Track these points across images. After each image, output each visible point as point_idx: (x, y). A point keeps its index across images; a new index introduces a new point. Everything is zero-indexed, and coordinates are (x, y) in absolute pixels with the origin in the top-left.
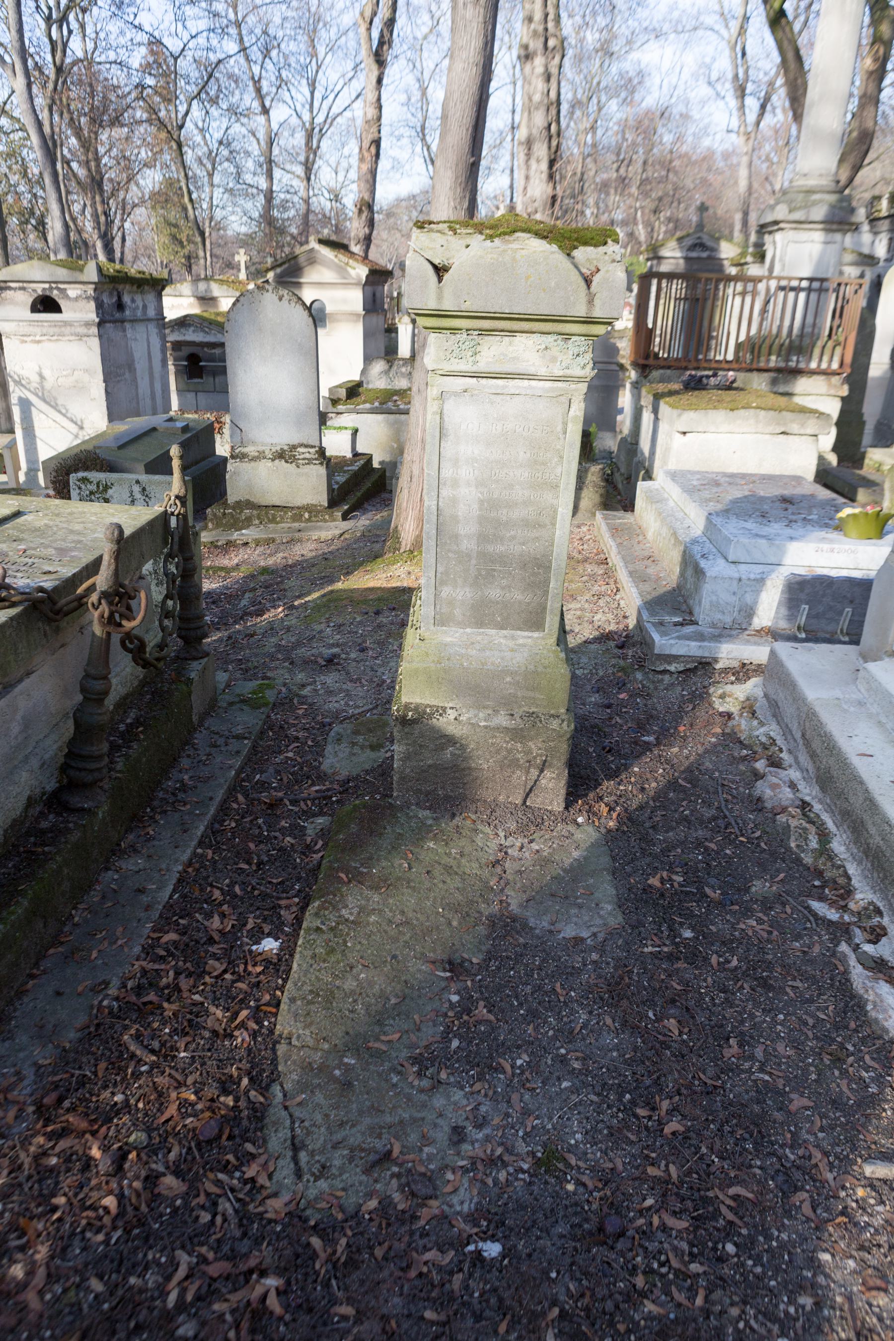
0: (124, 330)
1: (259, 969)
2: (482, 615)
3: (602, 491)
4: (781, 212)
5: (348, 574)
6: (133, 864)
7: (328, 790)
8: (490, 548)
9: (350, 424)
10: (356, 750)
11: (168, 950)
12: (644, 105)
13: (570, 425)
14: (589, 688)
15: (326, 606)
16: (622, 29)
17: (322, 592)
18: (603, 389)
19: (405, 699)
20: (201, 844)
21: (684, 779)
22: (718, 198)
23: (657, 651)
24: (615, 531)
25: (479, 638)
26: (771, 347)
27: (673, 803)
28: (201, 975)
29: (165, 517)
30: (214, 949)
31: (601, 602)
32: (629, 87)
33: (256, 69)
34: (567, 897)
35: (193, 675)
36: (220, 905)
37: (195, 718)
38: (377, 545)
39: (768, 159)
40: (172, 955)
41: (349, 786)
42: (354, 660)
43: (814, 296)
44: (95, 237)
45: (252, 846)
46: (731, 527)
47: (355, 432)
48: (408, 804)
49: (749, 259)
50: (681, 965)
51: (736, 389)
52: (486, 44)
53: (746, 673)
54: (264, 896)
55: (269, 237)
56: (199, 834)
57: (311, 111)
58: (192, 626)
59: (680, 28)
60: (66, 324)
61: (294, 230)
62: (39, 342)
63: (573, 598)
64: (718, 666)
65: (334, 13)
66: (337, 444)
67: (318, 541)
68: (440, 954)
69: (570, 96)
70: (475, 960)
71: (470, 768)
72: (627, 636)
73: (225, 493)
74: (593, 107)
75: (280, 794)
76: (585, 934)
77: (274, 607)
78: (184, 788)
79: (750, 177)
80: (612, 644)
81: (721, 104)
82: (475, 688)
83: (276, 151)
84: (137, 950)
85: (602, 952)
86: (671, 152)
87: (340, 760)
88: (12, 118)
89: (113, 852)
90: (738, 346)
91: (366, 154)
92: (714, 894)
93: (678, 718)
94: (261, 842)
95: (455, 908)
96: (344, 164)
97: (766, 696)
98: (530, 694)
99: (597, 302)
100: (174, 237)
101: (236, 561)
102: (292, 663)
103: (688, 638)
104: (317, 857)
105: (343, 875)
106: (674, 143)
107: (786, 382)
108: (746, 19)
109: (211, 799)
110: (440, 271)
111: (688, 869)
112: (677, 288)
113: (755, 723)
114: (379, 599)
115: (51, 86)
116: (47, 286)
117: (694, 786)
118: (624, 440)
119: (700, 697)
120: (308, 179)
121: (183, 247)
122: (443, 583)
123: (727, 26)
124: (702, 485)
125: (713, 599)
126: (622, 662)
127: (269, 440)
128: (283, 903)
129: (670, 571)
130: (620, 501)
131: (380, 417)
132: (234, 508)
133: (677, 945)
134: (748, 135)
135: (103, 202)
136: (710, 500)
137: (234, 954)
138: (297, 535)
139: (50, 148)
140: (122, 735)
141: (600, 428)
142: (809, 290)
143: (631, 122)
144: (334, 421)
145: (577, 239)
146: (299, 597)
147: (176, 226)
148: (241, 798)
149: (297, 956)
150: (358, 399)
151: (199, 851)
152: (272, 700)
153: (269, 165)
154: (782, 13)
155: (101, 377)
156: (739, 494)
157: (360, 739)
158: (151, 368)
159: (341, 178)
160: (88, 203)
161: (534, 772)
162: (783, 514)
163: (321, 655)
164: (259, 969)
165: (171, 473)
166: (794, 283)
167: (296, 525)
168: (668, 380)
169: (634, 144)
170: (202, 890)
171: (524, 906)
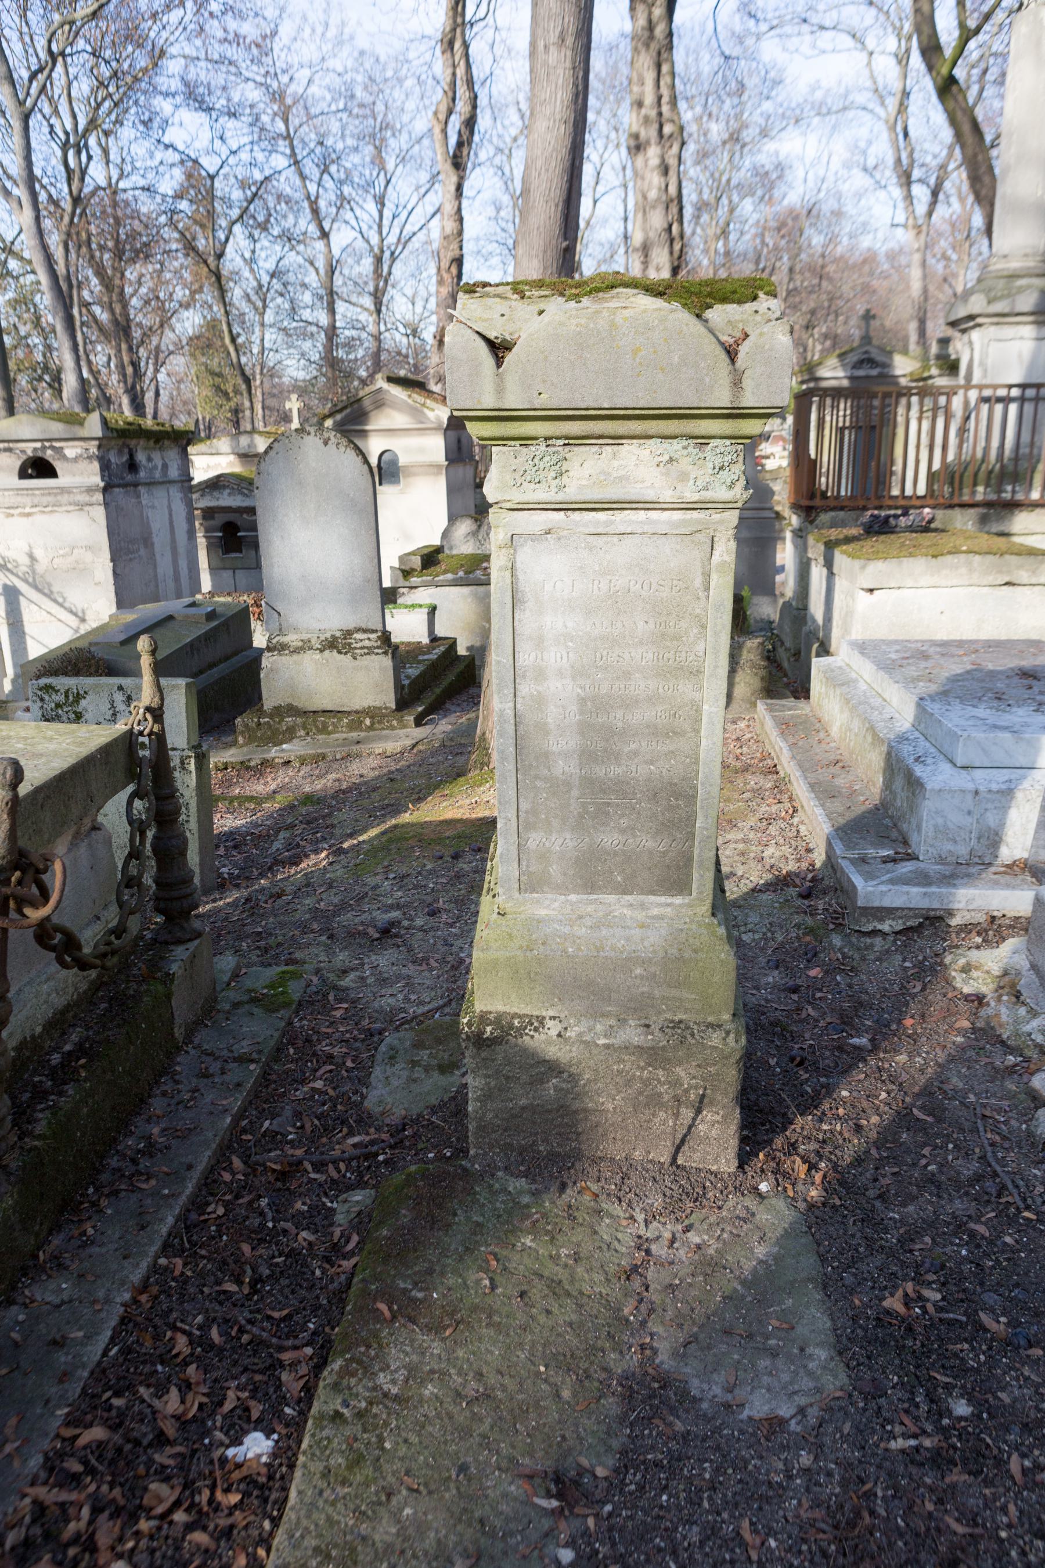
0: (138, 496)
1: (234, 1498)
2: (591, 874)
3: (763, 673)
4: (977, 304)
5: (420, 800)
6: (52, 1290)
7: (373, 1143)
8: (600, 771)
9: (428, 601)
10: (419, 1073)
11: (85, 1463)
12: (786, 202)
13: (714, 576)
14: (762, 961)
15: (385, 848)
16: (755, 117)
17: (383, 827)
18: (757, 532)
19: (479, 1007)
20: (166, 1248)
21: (921, 1108)
22: (885, 307)
23: (860, 904)
24: (786, 727)
25: (590, 909)
26: (976, 475)
27: (908, 1151)
28: (134, 1518)
29: (129, 739)
30: (162, 1457)
31: (773, 830)
32: (767, 182)
33: (312, 188)
34: (750, 1336)
35: (174, 968)
36: (186, 1364)
37: (179, 1033)
38: (458, 760)
39: (945, 257)
40: (91, 1471)
41: (404, 1135)
42: (421, 929)
43: (1029, 407)
44: (121, 391)
45: (246, 1248)
46: (955, 717)
47: (433, 610)
48: (490, 1170)
49: (934, 371)
50: (957, 1477)
51: (936, 530)
52: (577, 95)
53: (998, 931)
54: (257, 1344)
55: (333, 382)
56: (164, 1231)
57: (380, 233)
58: (175, 894)
59: (824, 110)
60: (63, 490)
61: (363, 373)
62: (29, 515)
63: (732, 824)
64: (954, 922)
65: (405, 118)
66: (407, 626)
67: (384, 755)
68: (541, 1462)
69: (694, 197)
70: (600, 1472)
71: (585, 1110)
72: (813, 880)
73: (260, 698)
74: (723, 211)
75: (299, 1152)
76: (785, 1411)
77: (316, 852)
78: (151, 1149)
79: (925, 277)
80: (793, 892)
81: (882, 194)
82: (589, 986)
83: (338, 280)
84: (35, 1462)
85: (818, 1450)
86: (823, 256)
87: (393, 1091)
88: (22, 259)
89: (24, 1271)
90: (931, 477)
91: (445, 276)
92: (997, 1325)
93: (901, 1002)
94: (261, 1241)
95: (563, 1362)
96: (423, 293)
97: (1034, 967)
98: (674, 993)
99: (747, 383)
100: (218, 389)
101: (273, 786)
102: (331, 937)
103: (906, 881)
104: (347, 1264)
105: (383, 1307)
106: (825, 246)
107: (1000, 519)
108: (906, 94)
109: (190, 1167)
110: (499, 349)
111: (948, 1278)
112: (843, 413)
113: (1022, 1011)
114: (459, 837)
115: (66, 219)
116: (38, 445)
117: (939, 1120)
118: (787, 605)
119: (931, 971)
120: (379, 311)
121: (229, 399)
122: (530, 827)
123: (883, 104)
124: (902, 658)
125: (939, 820)
126: (809, 920)
127: (316, 625)
128: (287, 1357)
129: (868, 780)
130: (787, 685)
131: (465, 590)
132: (271, 716)
133: (944, 1431)
134: (918, 228)
135: (130, 349)
136: (918, 679)
137: (197, 1466)
138: (355, 749)
139: (64, 295)
140: (53, 1074)
141: (754, 592)
142: (1022, 400)
143: (773, 224)
144: (407, 598)
145: (709, 295)
146: (351, 836)
147: (219, 375)
148: (237, 1163)
149: (298, 1473)
150: (438, 569)
151: (163, 1261)
152: (296, 997)
153: (330, 298)
154: (951, 80)
155: (108, 556)
156: (958, 669)
157: (424, 1055)
158: (173, 541)
159: (419, 309)
160: (112, 352)
161: (687, 1114)
162: (1026, 694)
163: (372, 923)
164: (234, 1498)
165: (137, 674)
166: (1002, 392)
167: (354, 735)
168: (843, 524)
169: (776, 248)
170: (157, 1337)
171: (680, 1354)
